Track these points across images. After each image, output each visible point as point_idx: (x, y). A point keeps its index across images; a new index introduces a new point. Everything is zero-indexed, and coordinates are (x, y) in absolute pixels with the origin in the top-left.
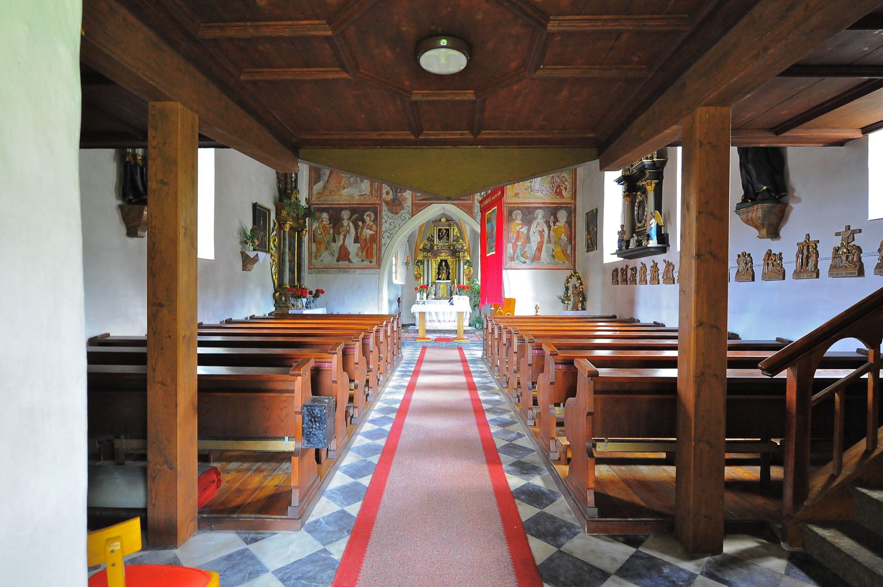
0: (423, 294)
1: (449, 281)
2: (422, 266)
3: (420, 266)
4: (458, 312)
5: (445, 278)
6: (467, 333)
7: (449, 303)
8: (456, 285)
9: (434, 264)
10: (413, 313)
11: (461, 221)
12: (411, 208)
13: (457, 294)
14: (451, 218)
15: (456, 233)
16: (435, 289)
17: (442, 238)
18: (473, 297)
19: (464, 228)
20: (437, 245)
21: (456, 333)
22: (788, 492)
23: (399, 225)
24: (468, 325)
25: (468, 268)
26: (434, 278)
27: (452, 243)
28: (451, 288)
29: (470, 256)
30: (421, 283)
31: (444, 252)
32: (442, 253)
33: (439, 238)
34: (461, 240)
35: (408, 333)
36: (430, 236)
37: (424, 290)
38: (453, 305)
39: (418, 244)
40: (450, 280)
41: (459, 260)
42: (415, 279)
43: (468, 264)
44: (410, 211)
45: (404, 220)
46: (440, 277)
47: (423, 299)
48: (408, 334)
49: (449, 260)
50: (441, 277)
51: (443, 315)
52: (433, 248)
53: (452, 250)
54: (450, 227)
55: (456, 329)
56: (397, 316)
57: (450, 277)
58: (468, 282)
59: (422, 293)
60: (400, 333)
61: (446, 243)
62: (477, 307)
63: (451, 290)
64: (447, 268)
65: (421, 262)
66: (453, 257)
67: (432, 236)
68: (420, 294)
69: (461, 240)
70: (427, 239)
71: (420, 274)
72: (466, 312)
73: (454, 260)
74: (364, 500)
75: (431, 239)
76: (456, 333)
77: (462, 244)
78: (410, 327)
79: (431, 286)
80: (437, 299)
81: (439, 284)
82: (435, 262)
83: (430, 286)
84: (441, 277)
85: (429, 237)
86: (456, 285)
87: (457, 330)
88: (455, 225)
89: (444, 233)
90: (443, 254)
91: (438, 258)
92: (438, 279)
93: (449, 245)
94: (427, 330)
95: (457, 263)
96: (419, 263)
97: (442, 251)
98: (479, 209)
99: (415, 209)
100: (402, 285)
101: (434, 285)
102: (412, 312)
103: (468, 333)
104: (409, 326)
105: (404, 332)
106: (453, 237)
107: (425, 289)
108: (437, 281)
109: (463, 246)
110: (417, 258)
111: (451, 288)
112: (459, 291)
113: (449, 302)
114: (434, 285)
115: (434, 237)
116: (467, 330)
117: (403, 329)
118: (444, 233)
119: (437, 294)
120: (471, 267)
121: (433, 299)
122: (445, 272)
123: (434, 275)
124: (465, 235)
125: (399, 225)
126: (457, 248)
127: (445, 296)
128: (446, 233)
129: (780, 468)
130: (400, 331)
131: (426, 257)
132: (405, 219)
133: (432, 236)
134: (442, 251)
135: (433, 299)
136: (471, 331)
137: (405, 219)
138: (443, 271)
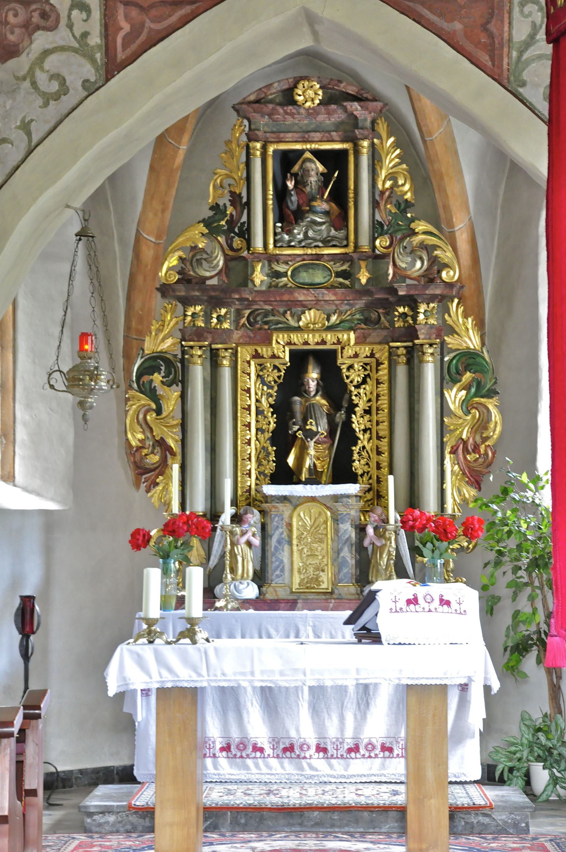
0: (181, 573)
1: (352, 489)
2: (174, 393)
3: (161, 391)
4: (409, 687)
5: (324, 466)
6: (471, 830)
7: (349, 631)
8: (393, 516)
9: (252, 383)
10: (121, 696)
11: (427, 104)
12: (96, 14)
13: (401, 573)
14: (356, 78)
15: (392, 177)
16: (257, 541)
17: (299, 215)
18: (504, 592)
19: (439, 148)
20: (272, 259)
21: (403, 831)
22: (470, 551)
23: (26, 127)
24: (478, 776)
25: (467, 406)
26: (252, 466)
27: (364, 241)
28: (361, 530)
29: (480, 325)
30: (167, 505)
31: (317, 304)
32: (306, 307)
33: (281, 217)
34: (421, 226)
35: (86, 830)
36: (225, 200)
37: (187, 545)
38: (376, 639)
39: (148, 254)
40: (352, 478)
41: (410, 351)
42: (131, 474)
43: (468, 376)
44: (95, 39)
45: (57, 96)
46: (291, 460)
47: (181, 602)
48: (82, 837)
49: (349, 352)
50: (300, 460)
51: (315, 710)
52: (246, 280)
53: (365, 291)
54: (355, 141)
55: (400, 799)
56: (18, 721)
57: (358, 466)
58: (469, 492)
59: (174, 565)
60: (32, 832)
61: (327, 243)
62: (534, 654)
63: (360, 548)
64: (335, 405)
65: (169, 363)
66: (376, 335)
67: (235, 198)
68: (165, 572)
69: (421, 226)
70: (207, 223)
71: (161, 443)
72: (464, 688)
73: (382, 354)
74: (323, 390)
75: (231, 223)
76: (403, 831)
77: (429, 249)
78: (102, 789)
79: (237, 519)
80: (274, 605)
81: (285, 509)
82: (262, 367)
83: (226, 518)
84: (300, 460)
85: (215, 207)
86: (393, 516)
87: (402, 811)
88: (382, 127)
89: (313, 179)
90: (309, 316)
91: (279, 339)
92: (276, 479)
93: (344, 258)
94: (206, 809)
95: (401, 371)
96: (157, 378)
97: (301, 296)
98: (540, 17)
99: (126, 27)
100: (46, 513)
101: (254, 517)
102: (112, 692)
103: (481, 831)
104: (95, 784)
105: (56, 828)
106: (375, 205)
107: (195, 542)
108: (270, 490)
109: (434, 261)
110: (142, 334)
111: (361, 530)
112: (415, 551)
113: (349, 621)
114: (254, 517)
115: (248, 204)
116: (475, 809)
117: (50, 805)
118: (313, 179)
119: (273, 574)
120: (491, 393)
121: (246, 604)
122: (322, 428)
123: (252, 449)
124: (452, 188)
125: (26, 127)
126: (400, 275)
127: (325, 585)
128: (326, 178)
129: (297, 441)
130: (32, 816)
131: (199, 334)
132: (64, 90)
133: (235, 198)
134: (301, 296)
135: (246, 604)
136: (500, 817)
137: (64, 90)
138: (311, 426)
